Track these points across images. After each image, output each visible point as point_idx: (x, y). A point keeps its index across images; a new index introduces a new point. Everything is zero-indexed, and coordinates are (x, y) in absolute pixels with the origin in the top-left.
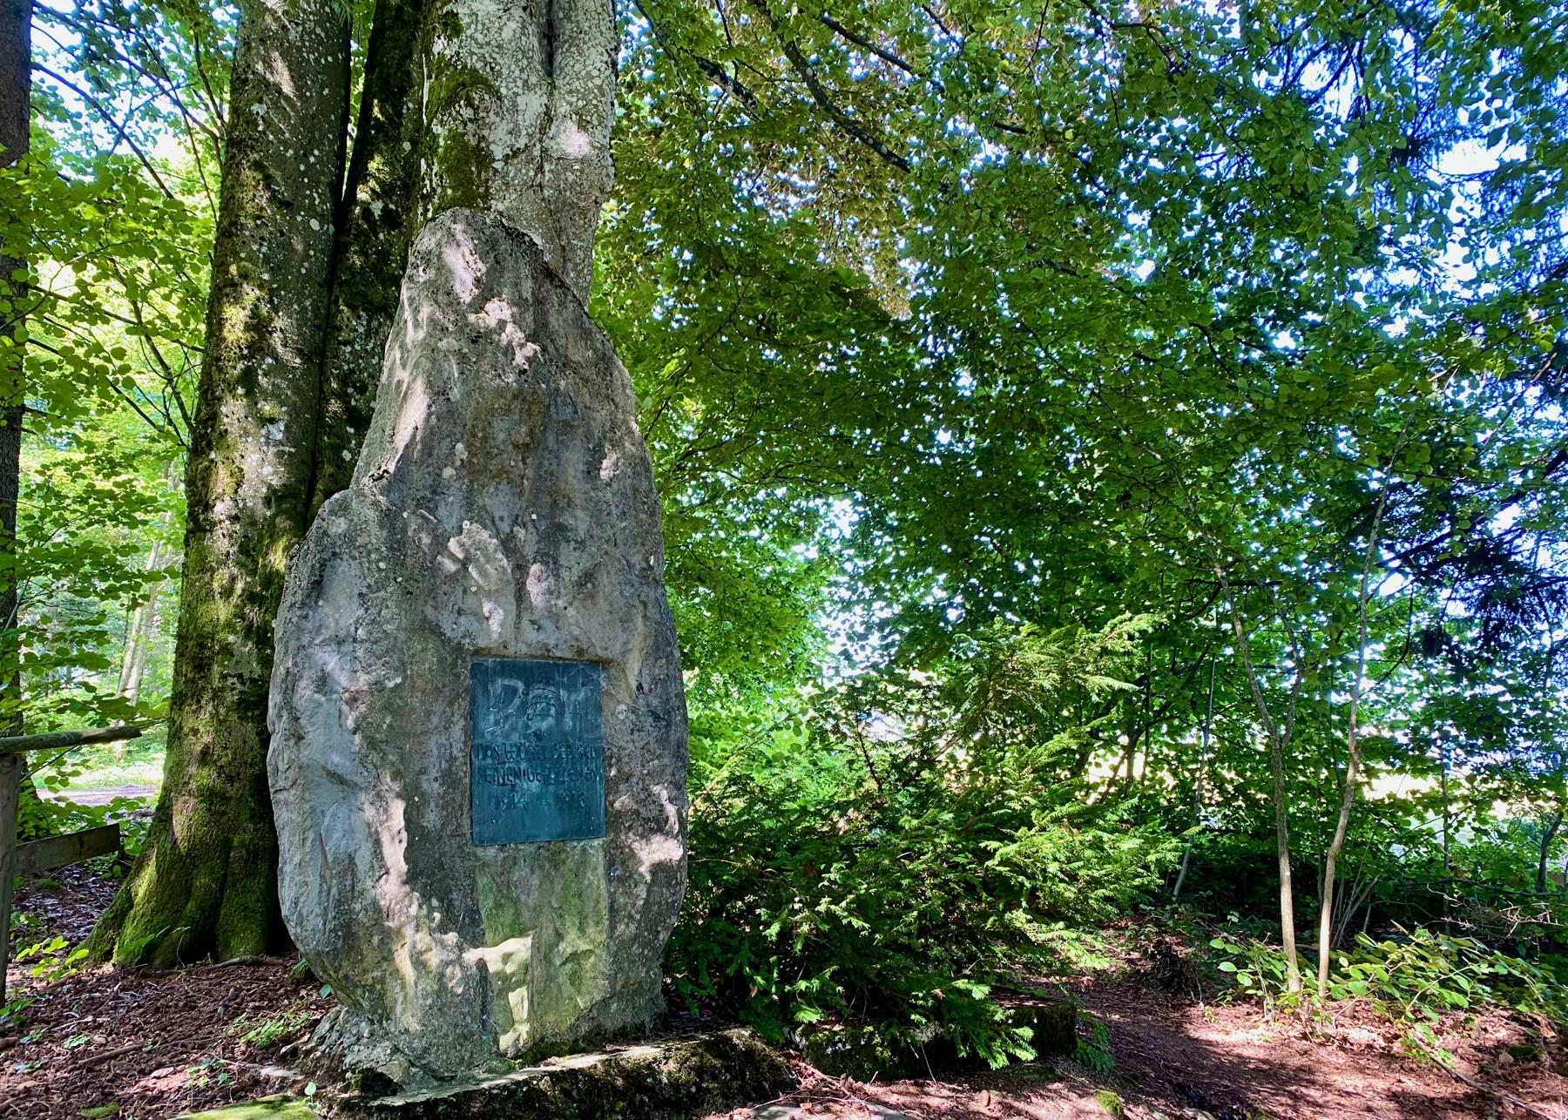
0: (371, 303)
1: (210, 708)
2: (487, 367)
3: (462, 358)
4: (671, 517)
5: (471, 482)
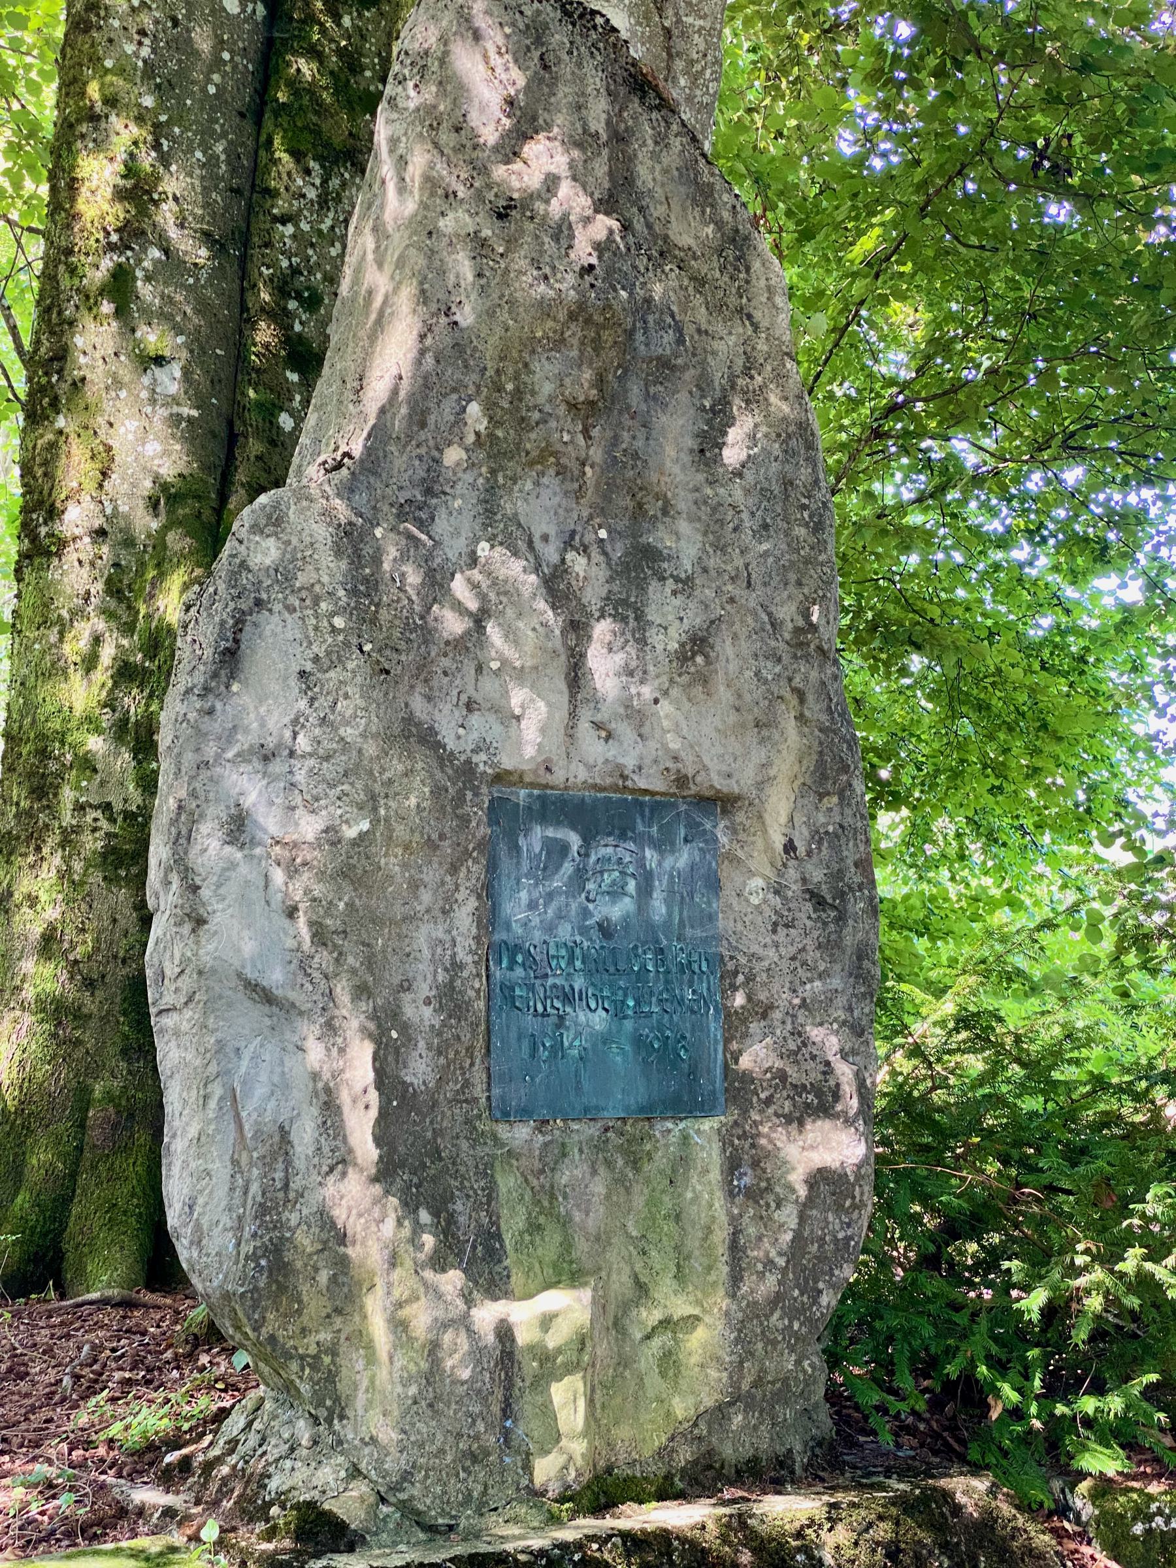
0: (327, 145)
1: (57, 860)
2: (523, 264)
3: (480, 246)
4: (859, 527)
5: (493, 472)
